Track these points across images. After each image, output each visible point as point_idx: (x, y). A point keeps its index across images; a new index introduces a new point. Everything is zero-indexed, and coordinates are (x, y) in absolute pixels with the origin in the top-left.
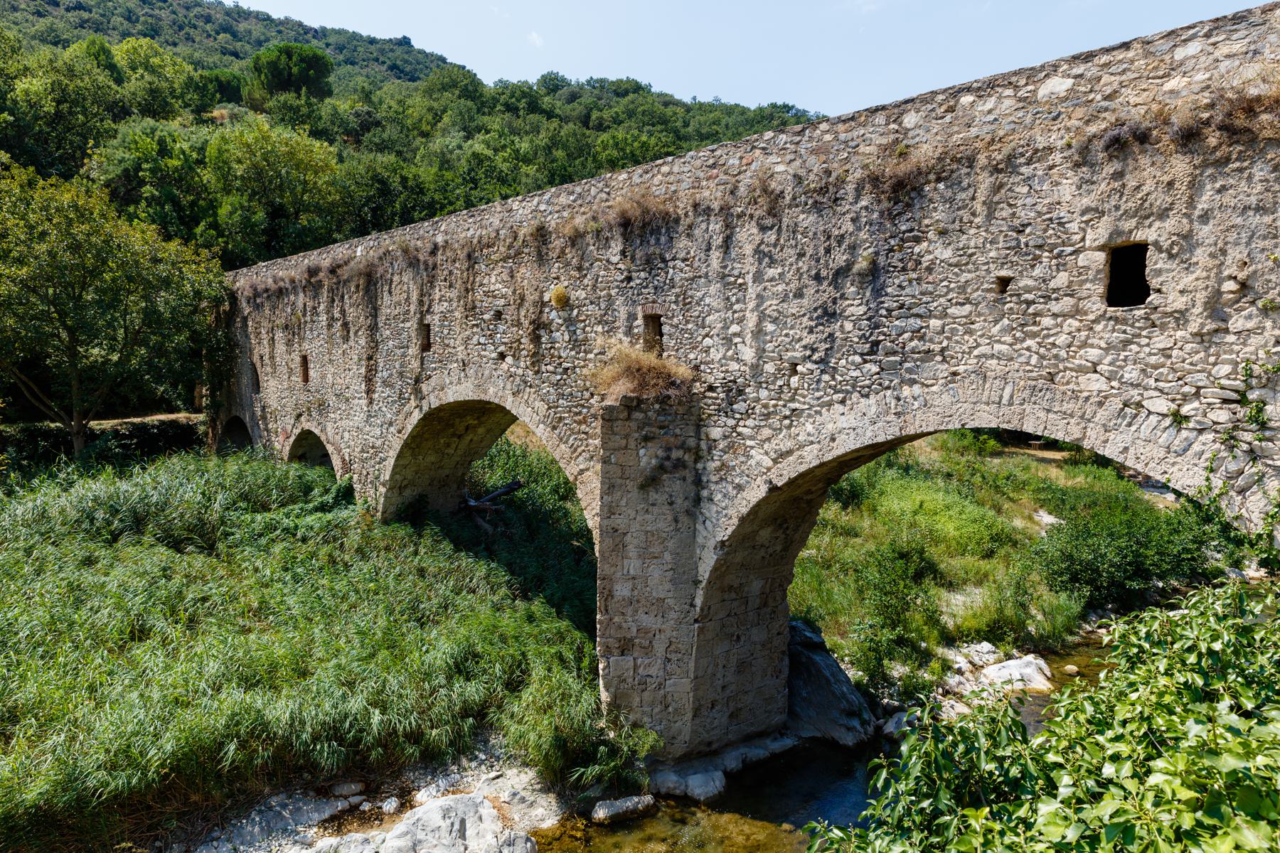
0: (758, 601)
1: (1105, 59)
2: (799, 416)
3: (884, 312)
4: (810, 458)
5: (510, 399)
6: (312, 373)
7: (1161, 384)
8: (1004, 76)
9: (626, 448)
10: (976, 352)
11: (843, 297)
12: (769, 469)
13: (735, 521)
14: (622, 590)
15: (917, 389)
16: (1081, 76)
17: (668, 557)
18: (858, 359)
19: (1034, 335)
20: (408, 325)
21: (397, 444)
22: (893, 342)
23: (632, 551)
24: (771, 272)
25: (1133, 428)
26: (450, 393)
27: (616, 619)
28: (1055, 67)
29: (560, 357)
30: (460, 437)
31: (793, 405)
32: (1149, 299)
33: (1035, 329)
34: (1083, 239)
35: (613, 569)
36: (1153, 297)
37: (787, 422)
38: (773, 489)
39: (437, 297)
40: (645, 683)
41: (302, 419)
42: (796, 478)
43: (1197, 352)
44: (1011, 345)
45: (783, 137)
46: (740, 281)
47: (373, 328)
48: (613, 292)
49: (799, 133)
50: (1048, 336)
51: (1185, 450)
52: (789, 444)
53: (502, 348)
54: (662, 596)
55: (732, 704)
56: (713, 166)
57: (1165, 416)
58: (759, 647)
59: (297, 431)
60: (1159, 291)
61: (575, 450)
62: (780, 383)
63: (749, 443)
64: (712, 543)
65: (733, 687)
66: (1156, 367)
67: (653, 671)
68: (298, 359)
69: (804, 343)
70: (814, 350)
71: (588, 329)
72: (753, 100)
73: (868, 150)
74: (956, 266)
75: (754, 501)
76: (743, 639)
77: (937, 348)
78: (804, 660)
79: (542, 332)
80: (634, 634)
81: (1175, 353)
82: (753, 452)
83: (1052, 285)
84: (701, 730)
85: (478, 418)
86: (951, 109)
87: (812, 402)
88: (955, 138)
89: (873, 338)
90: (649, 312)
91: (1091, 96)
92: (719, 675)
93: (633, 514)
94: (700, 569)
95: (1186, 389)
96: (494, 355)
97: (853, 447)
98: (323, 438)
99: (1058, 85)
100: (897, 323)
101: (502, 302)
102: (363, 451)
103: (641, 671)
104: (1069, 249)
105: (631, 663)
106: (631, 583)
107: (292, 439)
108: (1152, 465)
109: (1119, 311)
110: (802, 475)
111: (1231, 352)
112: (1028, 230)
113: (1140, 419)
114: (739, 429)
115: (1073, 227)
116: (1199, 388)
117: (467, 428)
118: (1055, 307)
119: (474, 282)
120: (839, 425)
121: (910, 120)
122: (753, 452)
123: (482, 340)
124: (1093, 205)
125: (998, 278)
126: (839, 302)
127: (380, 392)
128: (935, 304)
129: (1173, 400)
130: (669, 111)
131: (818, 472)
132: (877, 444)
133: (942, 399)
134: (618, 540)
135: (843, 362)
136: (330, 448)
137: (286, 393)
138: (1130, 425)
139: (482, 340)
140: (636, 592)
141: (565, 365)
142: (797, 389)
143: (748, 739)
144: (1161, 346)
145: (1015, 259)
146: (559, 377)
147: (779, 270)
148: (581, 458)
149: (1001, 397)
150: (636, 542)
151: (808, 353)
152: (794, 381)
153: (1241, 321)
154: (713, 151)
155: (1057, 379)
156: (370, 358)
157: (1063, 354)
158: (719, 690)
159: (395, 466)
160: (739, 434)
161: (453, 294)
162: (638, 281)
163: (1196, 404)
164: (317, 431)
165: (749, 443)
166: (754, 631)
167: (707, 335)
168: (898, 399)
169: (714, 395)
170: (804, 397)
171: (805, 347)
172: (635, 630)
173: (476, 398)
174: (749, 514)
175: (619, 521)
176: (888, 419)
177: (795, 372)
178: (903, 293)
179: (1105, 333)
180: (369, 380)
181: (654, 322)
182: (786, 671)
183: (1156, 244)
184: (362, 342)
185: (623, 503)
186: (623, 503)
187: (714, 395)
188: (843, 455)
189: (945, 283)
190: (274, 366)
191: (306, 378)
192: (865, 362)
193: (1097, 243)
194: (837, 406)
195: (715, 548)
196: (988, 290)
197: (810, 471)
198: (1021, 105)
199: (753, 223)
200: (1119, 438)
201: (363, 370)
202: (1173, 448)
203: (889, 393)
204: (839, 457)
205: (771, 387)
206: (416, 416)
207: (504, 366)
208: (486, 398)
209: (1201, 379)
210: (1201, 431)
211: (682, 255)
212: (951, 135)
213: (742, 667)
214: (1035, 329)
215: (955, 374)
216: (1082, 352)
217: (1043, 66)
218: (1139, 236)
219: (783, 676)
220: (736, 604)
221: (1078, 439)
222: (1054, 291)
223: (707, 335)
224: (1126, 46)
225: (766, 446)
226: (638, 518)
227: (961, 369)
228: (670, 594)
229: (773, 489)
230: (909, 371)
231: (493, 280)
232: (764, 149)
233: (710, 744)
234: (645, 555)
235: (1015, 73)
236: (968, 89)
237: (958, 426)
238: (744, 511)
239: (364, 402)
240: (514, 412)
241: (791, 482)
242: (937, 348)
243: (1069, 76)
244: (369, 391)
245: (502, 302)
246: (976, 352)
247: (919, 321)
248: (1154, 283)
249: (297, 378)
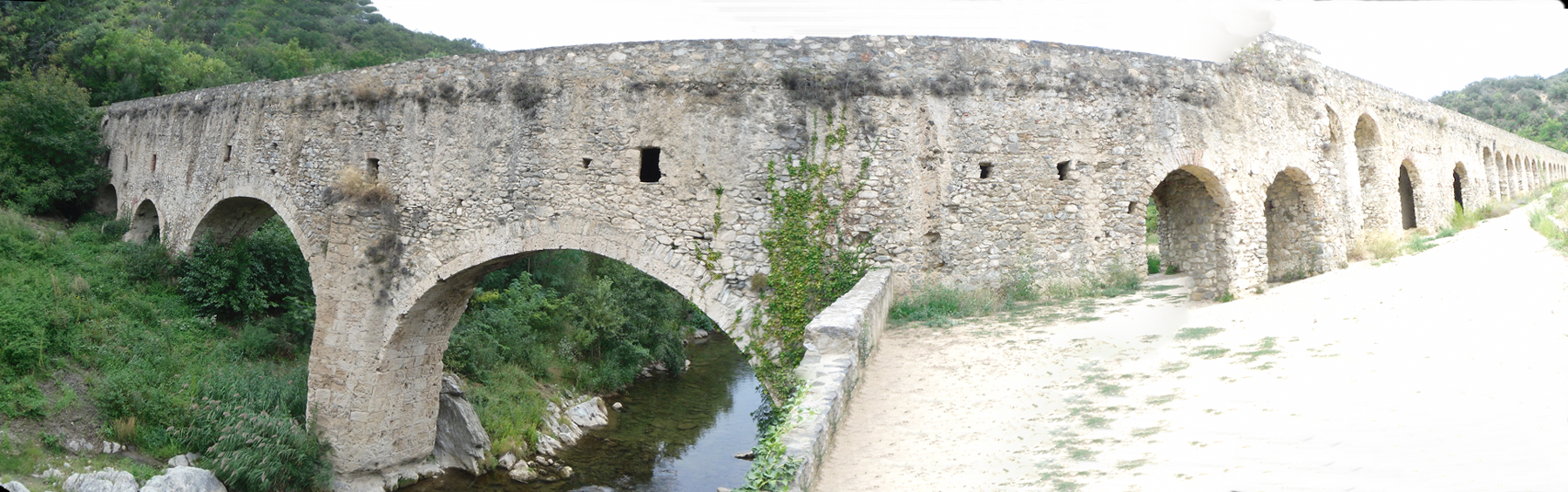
0: (422, 360)
1: (642, 47)
2: (461, 234)
3: (517, 172)
4: (465, 263)
5: (274, 200)
6: (157, 166)
7: (666, 228)
8: (592, 46)
9: (345, 243)
10: (569, 202)
11: (494, 160)
12: (439, 267)
13: (414, 302)
14: (330, 341)
15: (535, 222)
16: (630, 54)
17: (364, 321)
18: (500, 200)
19: (601, 194)
20: (218, 144)
21: (199, 219)
22: (521, 191)
23: (340, 314)
24: (451, 140)
25: (651, 252)
26: (237, 191)
27: (323, 361)
28: (617, 46)
29: (310, 178)
30: (239, 219)
31: (457, 226)
32: (660, 179)
33: (603, 191)
34: (628, 142)
35: (326, 324)
36: (662, 179)
37: (453, 237)
38: (440, 281)
39: (239, 130)
40: (337, 411)
41: (147, 192)
42: (455, 275)
43: (683, 210)
44: (589, 199)
45: (464, 59)
46: (430, 143)
47: (197, 144)
48: (350, 142)
49: (471, 59)
50: (609, 195)
51: (677, 265)
52: (453, 253)
53: (274, 167)
54: (357, 349)
55: (396, 435)
56: (419, 71)
57: (667, 245)
58: (419, 393)
59: (143, 199)
60: (665, 175)
61: (311, 240)
62: (451, 210)
63: (427, 249)
64: (396, 315)
65: (397, 422)
66: (662, 217)
67: (343, 403)
68: (151, 156)
69: (467, 187)
70: (473, 192)
71: (330, 162)
72: (452, 35)
73: (514, 74)
74: (561, 149)
75: (427, 288)
76: (409, 386)
77: (548, 198)
78: (450, 405)
79: (301, 160)
80: (334, 374)
81: (672, 210)
82: (429, 255)
83: (613, 166)
84: (371, 452)
85: (252, 209)
86: (562, 59)
87: (471, 226)
88: (564, 75)
89: (509, 188)
90: (371, 157)
91: (635, 65)
92: (389, 413)
93: (344, 288)
94: (385, 333)
95: (678, 230)
96: (269, 171)
97: (493, 257)
98: (156, 206)
99: (619, 57)
100: (525, 180)
101: (278, 138)
102: (178, 218)
103: (335, 401)
104: (622, 147)
105: (328, 396)
106: (337, 336)
107: (139, 203)
108: (660, 274)
109: (645, 184)
110: (459, 273)
111: (698, 211)
112: (601, 133)
113: (655, 247)
114: (423, 239)
115: (624, 135)
116: (683, 230)
117: (244, 214)
118: (614, 179)
119: (263, 123)
120: (486, 242)
121: (540, 61)
122: (429, 255)
123: (262, 160)
124: (634, 124)
125: (584, 159)
126: (491, 163)
127: (194, 183)
128: (548, 171)
129: (671, 236)
130: (397, 34)
131: (470, 272)
132: (508, 256)
133: (548, 230)
134: (332, 305)
135: (491, 202)
136: (159, 213)
137: (141, 175)
138: (650, 250)
139: (262, 160)
140: (339, 344)
141: (312, 183)
142: (461, 216)
143: (404, 463)
144: (666, 206)
145: (593, 149)
146: (307, 190)
147: (456, 140)
148: (314, 246)
149: (582, 230)
150: (344, 308)
151: (470, 193)
152: (459, 211)
153: (702, 195)
154: (421, 62)
155: (613, 221)
156: (192, 162)
157: (617, 206)
158: (388, 423)
159: (196, 231)
160: (421, 242)
161: (248, 129)
162: (366, 137)
163: (681, 239)
164: (154, 202)
165: (427, 249)
166: (417, 381)
167: (407, 175)
168: (523, 228)
169: (407, 214)
170: (465, 221)
171: (468, 189)
172: (335, 371)
173: (254, 197)
174: (422, 297)
175: (334, 292)
176: (516, 240)
177: (460, 205)
178: (530, 162)
179: (640, 195)
180: (189, 175)
181: (374, 162)
182: (437, 412)
183: (664, 149)
184: (190, 151)
185: (339, 280)
186: (339, 280)
187: (407, 214)
188: (487, 262)
189: (554, 159)
190: (136, 158)
191: (154, 168)
192: (505, 202)
193: (635, 145)
194: (485, 229)
195: (397, 319)
196: (579, 165)
197: (466, 271)
198: (599, 63)
199: (442, 109)
200: (645, 258)
201: (187, 169)
202: (671, 264)
203: (517, 223)
204: (484, 263)
205: (445, 213)
206: (214, 202)
207: (273, 179)
208: (259, 198)
209: (683, 225)
210: (684, 254)
211: (396, 124)
212: (561, 73)
213: (407, 406)
214: (603, 191)
215: (556, 214)
216: (627, 206)
217: (611, 45)
218: (656, 144)
219: (433, 417)
220: (407, 360)
221: (624, 259)
222: (613, 169)
223: (407, 175)
224: (651, 43)
225: (438, 253)
226: (348, 292)
227: (560, 212)
228: (362, 349)
229: (440, 281)
230: (530, 210)
231: (275, 124)
232: (452, 65)
233: (377, 464)
234: (350, 319)
235: (597, 45)
236: (572, 49)
237: (558, 248)
238: (420, 295)
239: (184, 188)
240: (275, 209)
241: (453, 277)
242: (548, 198)
243: (624, 53)
244: (188, 182)
245: (278, 138)
246: (569, 202)
247: (538, 180)
248: (663, 171)
249: (148, 167)
